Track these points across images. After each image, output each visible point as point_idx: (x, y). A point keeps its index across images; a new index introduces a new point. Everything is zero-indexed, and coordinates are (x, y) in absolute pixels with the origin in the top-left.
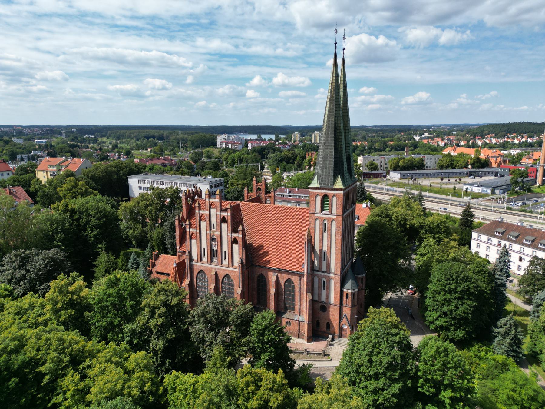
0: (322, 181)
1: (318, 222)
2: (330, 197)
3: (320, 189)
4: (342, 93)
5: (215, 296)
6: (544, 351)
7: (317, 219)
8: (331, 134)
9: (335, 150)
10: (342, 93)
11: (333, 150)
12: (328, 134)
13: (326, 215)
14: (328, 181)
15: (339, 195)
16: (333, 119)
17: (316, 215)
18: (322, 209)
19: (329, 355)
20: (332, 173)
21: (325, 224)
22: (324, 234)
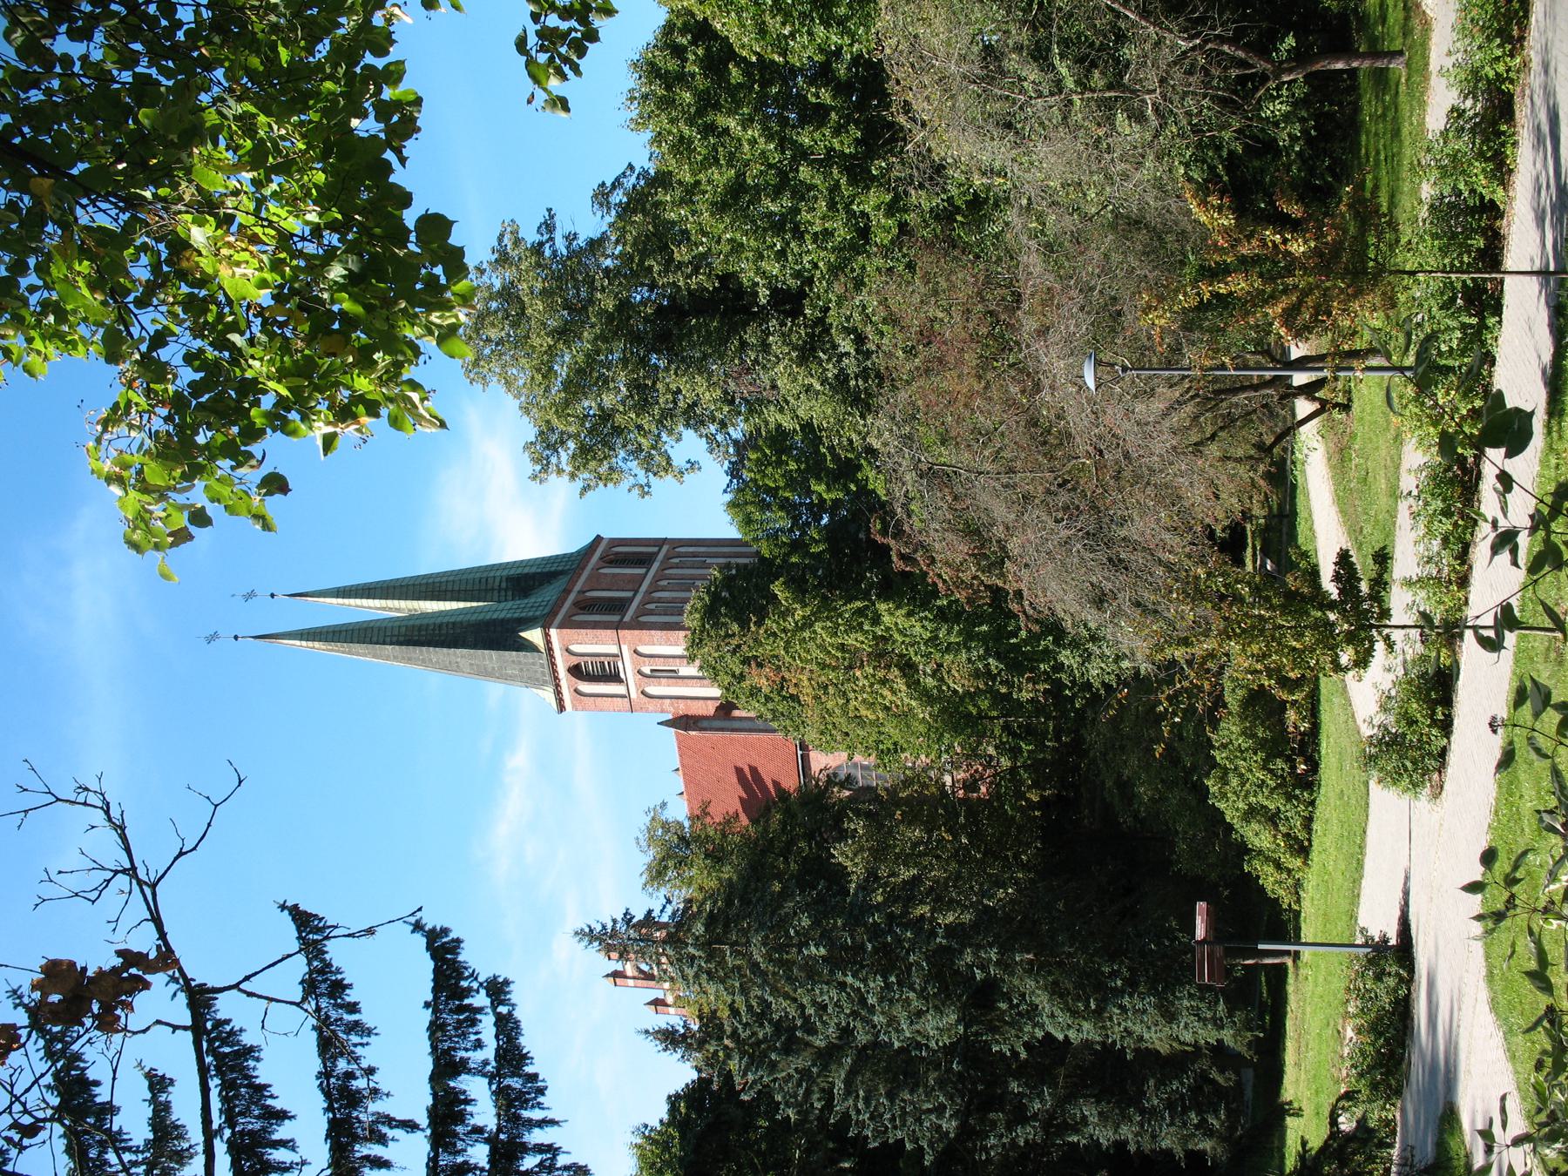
0: (537, 680)
1: (651, 690)
2: (574, 661)
3: (557, 686)
4: (691, 549)
5: (897, 330)
6: (638, 1122)
7: (643, 693)
8: (422, 654)
9: (456, 647)
10: (691, 549)
11: (459, 651)
12: (423, 661)
13: (628, 668)
14: (533, 664)
15: (561, 640)
16: (390, 648)
17: (634, 695)
18: (615, 677)
19: (1524, 1033)
20: (512, 655)
21: (652, 671)
22: (680, 674)
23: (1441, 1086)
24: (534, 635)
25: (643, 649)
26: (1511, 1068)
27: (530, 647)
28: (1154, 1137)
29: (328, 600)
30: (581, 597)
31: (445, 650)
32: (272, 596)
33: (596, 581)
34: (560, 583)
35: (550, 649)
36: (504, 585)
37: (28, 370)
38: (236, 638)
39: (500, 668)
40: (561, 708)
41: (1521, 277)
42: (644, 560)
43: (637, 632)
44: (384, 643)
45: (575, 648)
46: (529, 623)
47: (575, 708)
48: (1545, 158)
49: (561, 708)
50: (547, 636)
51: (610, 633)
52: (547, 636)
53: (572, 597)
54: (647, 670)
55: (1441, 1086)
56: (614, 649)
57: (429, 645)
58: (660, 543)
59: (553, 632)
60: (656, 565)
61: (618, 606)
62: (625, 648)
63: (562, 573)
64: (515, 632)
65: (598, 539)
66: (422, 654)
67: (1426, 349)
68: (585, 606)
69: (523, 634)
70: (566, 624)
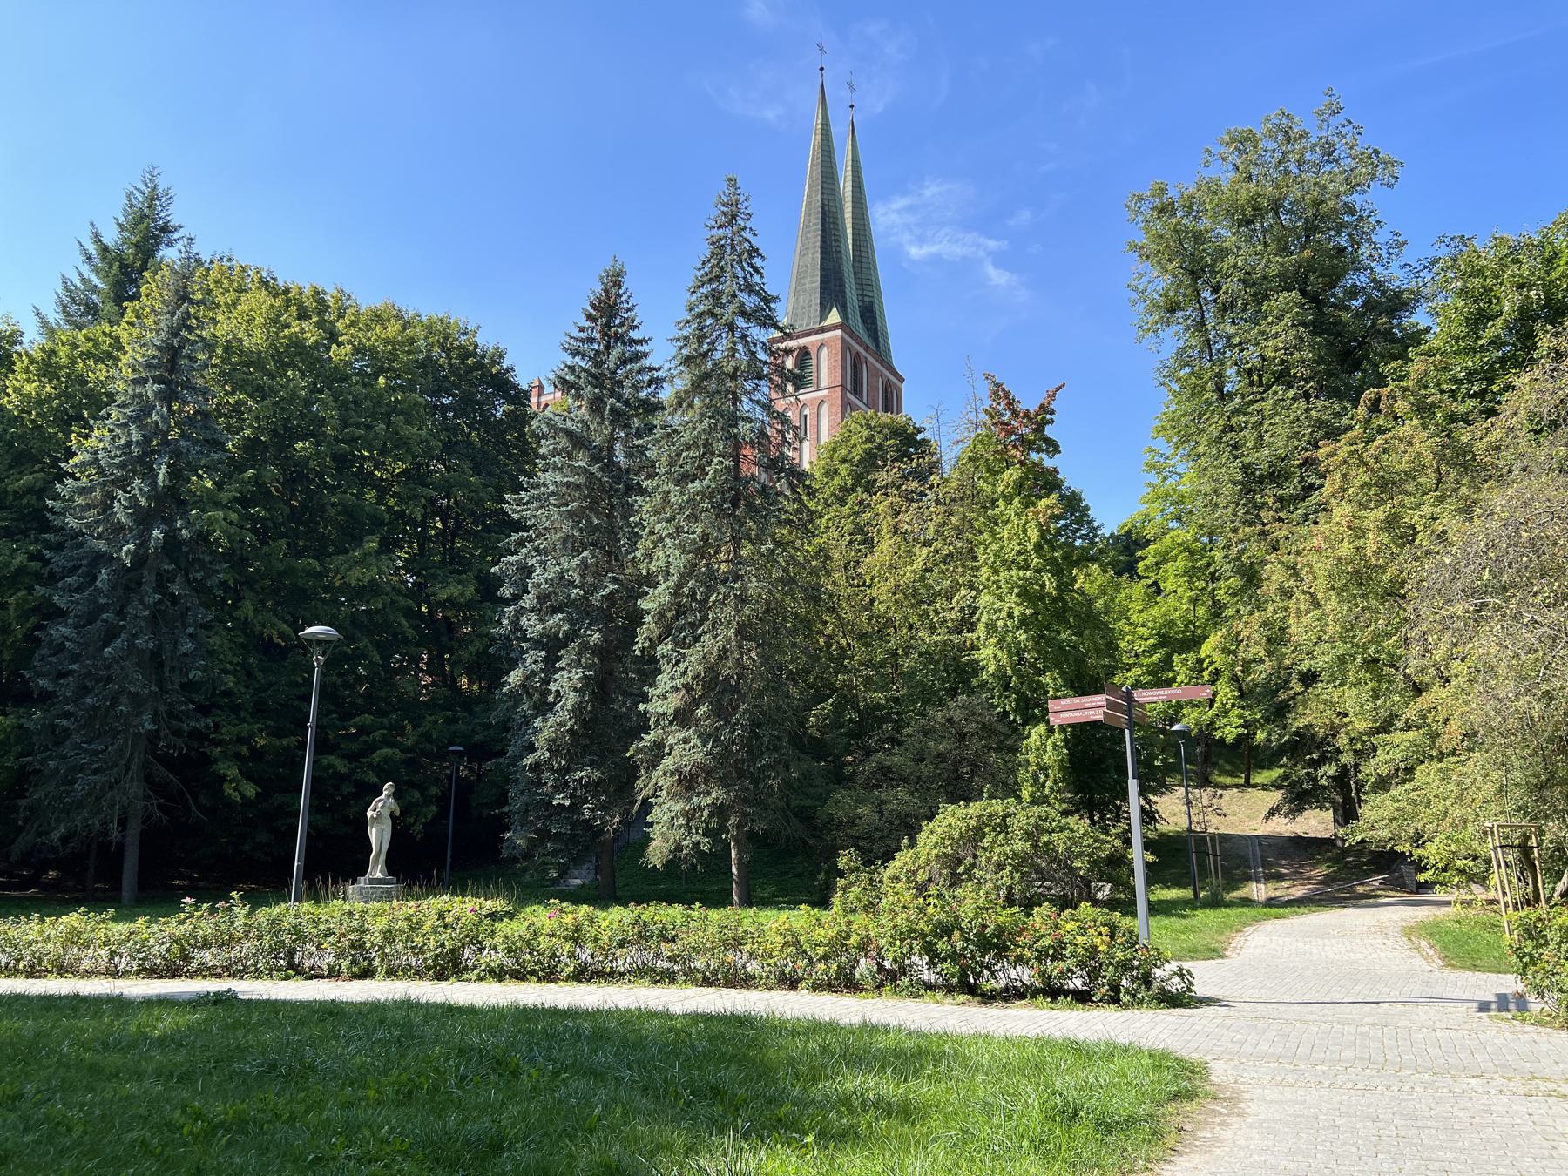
2: (813, 353)
14: (809, 318)
15: (832, 339)
16: (819, 198)
20: (816, 299)
24: (834, 317)
25: (825, 408)
26: (1000, 1004)
27: (824, 314)
28: (1517, 785)
29: (850, 153)
30: (863, 360)
31: (819, 244)
32: (852, 106)
33: (874, 373)
34: (872, 347)
35: (823, 330)
36: (866, 299)
38: (822, 69)
39: (805, 290)
43: (839, 402)
44: (822, 193)
45: (825, 352)
46: (843, 312)
50: (833, 327)
51: (838, 381)
52: (833, 327)
54: (807, 411)
56: (824, 384)
57: (823, 230)
59: (838, 332)
61: (857, 390)
62: (826, 392)
63: (876, 340)
65: (902, 380)
66: (815, 224)
67: (610, 673)
69: (835, 309)
70: (845, 346)
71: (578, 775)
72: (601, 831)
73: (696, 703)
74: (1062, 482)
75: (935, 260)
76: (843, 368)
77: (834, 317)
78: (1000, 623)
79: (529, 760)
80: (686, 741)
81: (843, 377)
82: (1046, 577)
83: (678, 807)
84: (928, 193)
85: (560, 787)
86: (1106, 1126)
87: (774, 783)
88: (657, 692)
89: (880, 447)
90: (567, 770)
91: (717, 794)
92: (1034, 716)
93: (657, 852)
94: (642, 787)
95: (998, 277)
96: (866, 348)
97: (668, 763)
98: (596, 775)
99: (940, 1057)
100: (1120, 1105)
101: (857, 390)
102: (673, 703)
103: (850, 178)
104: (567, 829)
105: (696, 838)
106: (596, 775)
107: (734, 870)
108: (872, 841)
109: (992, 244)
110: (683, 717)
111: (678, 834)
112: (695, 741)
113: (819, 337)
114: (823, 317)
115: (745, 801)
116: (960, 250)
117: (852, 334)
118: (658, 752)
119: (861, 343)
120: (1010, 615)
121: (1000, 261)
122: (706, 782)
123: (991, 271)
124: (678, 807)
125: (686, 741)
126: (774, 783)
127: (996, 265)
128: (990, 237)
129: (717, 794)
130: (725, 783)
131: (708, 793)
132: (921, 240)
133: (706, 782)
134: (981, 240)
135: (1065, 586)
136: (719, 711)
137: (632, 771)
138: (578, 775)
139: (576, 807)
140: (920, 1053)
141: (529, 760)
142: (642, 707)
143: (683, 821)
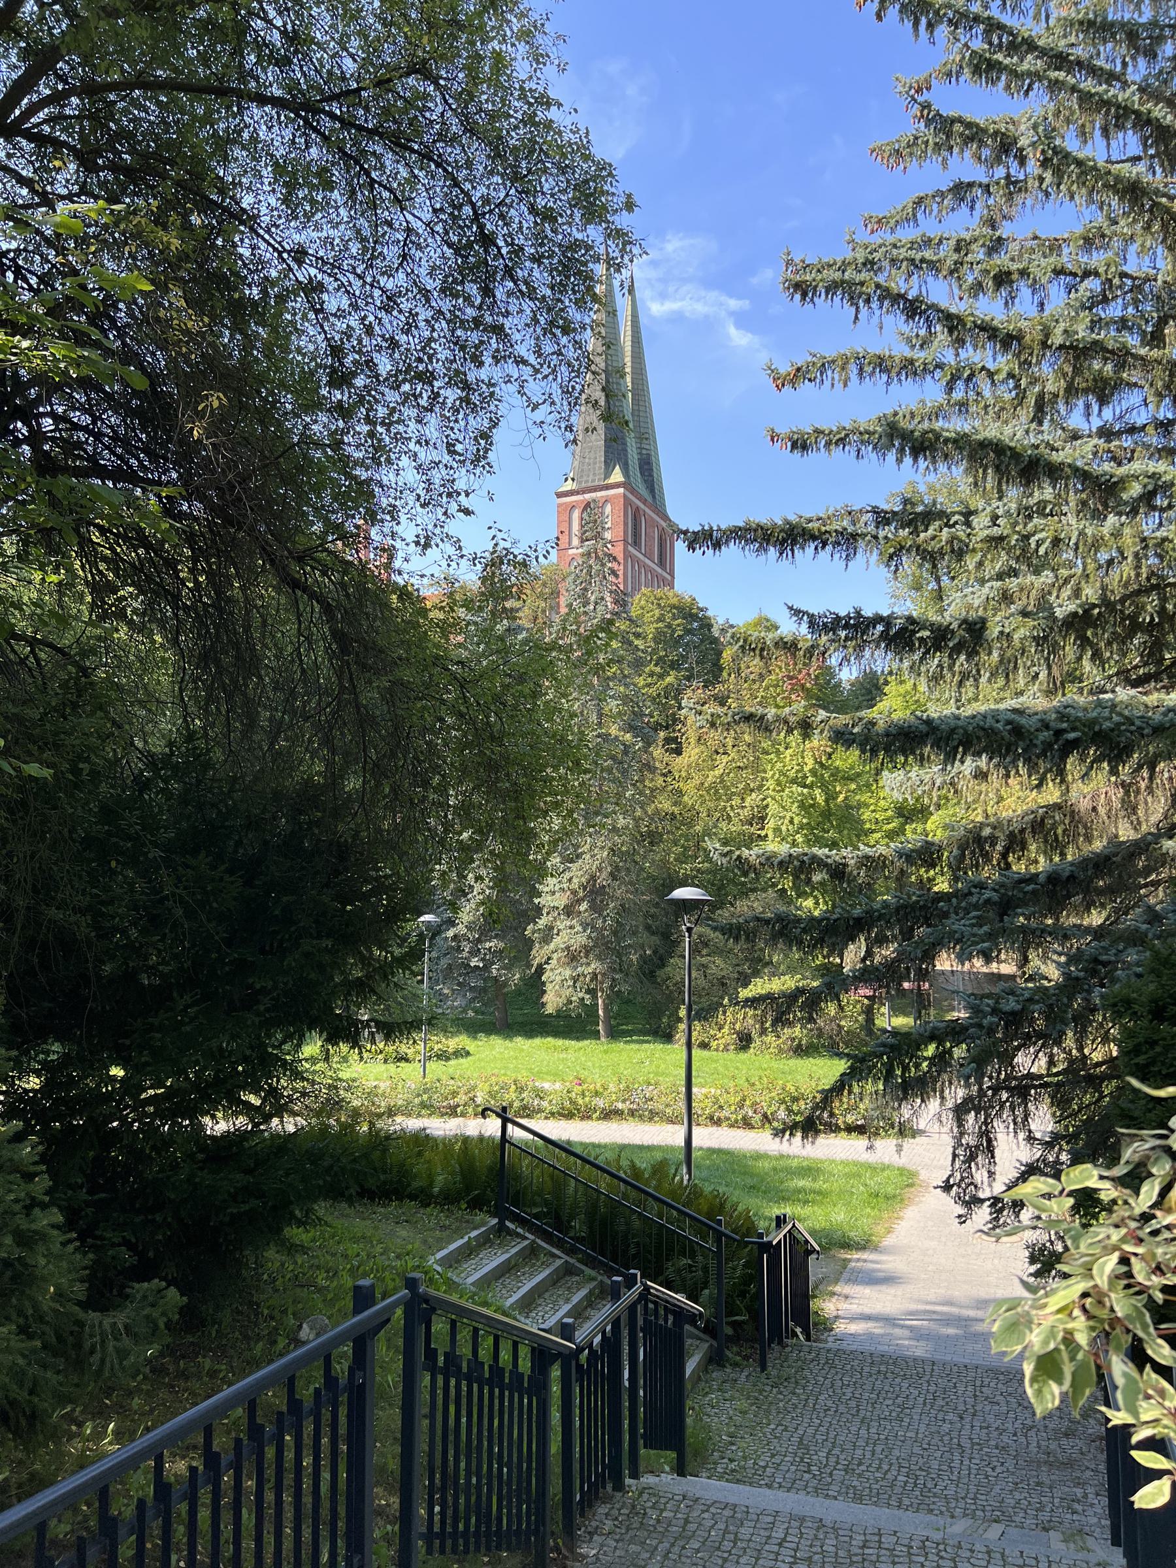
15: (616, 496)
17: (571, 552)
23: (484, 1505)
24: (617, 476)
33: (651, 524)
34: (650, 499)
37: (587, 133)
40: (560, 495)
41: (682, 1072)
42: (662, 563)
46: (626, 472)
47: (559, 506)
48: (928, 1303)
49: (560, 495)
50: (617, 485)
52: (617, 485)
53: (642, 506)
55: (484, 1505)
58: (672, 574)
59: (621, 490)
60: (659, 570)
61: (636, 543)
63: (652, 490)
64: (619, 460)
68: (636, 515)
70: (627, 502)
71: (488, 945)
72: (505, 984)
73: (579, 901)
74: (788, 522)
75: (677, 318)
76: (626, 524)
77: (617, 476)
78: (784, 828)
79: (450, 933)
80: (571, 927)
81: (625, 532)
82: (817, 792)
83: (568, 973)
84: (670, 247)
85: (474, 952)
86: (887, 1198)
87: (634, 958)
88: (546, 889)
89: (669, 626)
90: (479, 941)
91: (595, 966)
92: (805, 892)
93: (552, 1001)
94: (538, 954)
95: (738, 338)
96: (645, 502)
97: (558, 942)
98: (501, 945)
99: (818, 1170)
100: (890, 1190)
101: (636, 543)
102: (561, 900)
103: (629, 328)
104: (481, 983)
105: (581, 995)
106: (501, 945)
107: (601, 1012)
108: (700, 996)
109: (733, 304)
110: (569, 911)
111: (568, 992)
112: (579, 928)
113: (603, 493)
114: (607, 475)
115: (614, 970)
116: (700, 308)
117: (633, 491)
118: (548, 934)
119: (640, 498)
120: (791, 822)
121: (742, 320)
122: (587, 956)
123: (732, 331)
124: (568, 973)
125: (571, 927)
126: (634, 958)
127: (738, 326)
128: (731, 297)
129: (595, 966)
130: (599, 958)
131: (588, 964)
132: (663, 296)
133: (587, 956)
134: (723, 298)
135: (830, 797)
136: (593, 907)
137: (529, 944)
138: (488, 945)
139: (487, 968)
140: (809, 1169)
141: (450, 933)
142: (536, 901)
143: (571, 983)
